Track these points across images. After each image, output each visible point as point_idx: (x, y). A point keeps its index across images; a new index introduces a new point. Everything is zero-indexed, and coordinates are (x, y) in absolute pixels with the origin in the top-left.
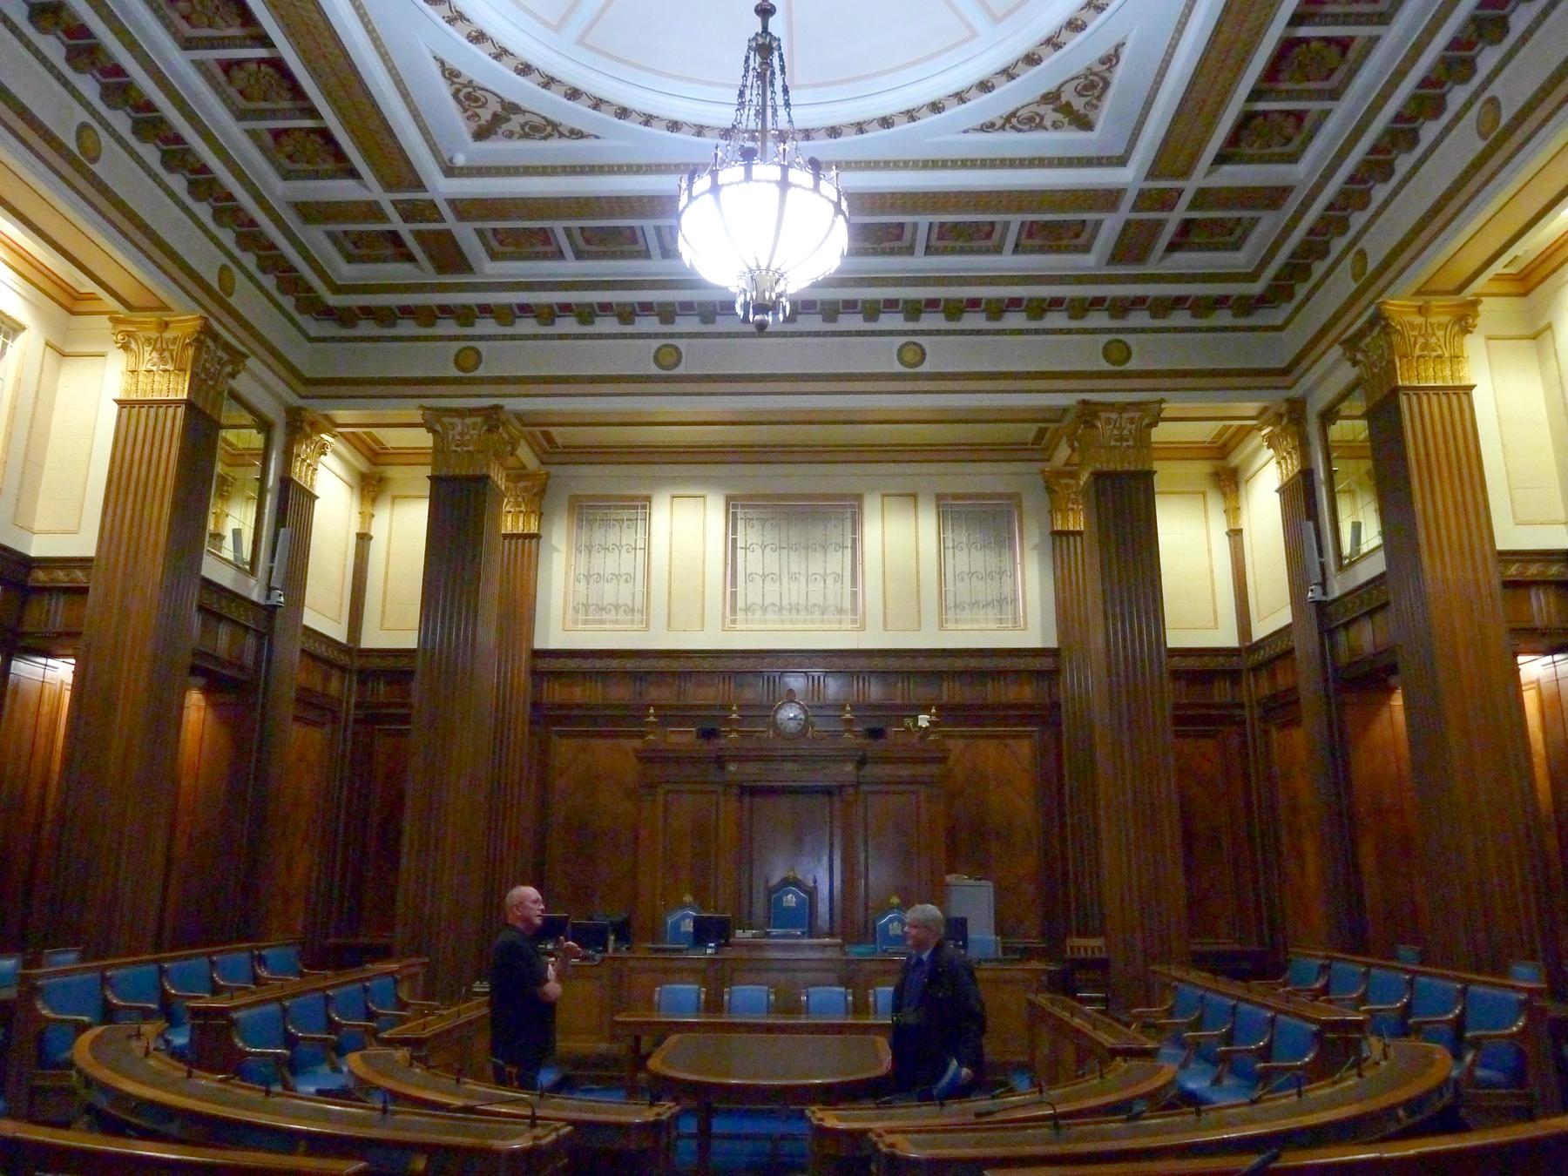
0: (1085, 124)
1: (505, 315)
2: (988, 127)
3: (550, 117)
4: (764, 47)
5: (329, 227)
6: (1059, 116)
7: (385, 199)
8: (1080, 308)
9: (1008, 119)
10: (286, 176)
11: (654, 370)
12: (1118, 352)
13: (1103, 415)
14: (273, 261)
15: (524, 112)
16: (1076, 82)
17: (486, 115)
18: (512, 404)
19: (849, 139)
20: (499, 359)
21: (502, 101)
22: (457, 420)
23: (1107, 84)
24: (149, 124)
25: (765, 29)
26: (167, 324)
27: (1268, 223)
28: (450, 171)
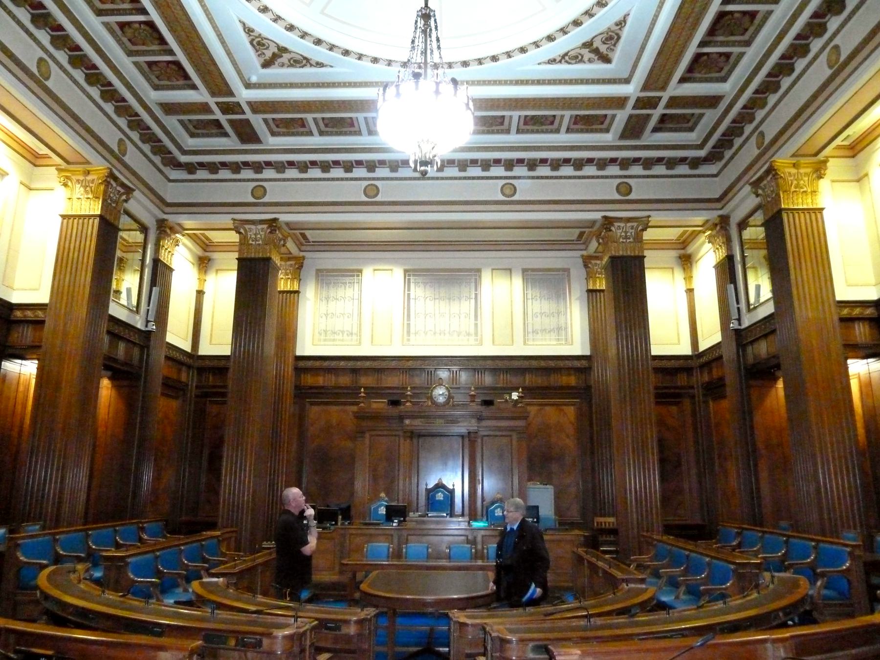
0: (606, 60)
1: (280, 167)
2: (552, 61)
3: (305, 55)
6: (592, 56)
7: (212, 101)
8: (602, 164)
9: (563, 57)
12: (625, 189)
13: (616, 224)
14: (148, 137)
15: (290, 52)
17: (268, 54)
20: (275, 192)
22: (253, 227)
23: (619, 38)
24: (79, 60)
28: (248, 86)
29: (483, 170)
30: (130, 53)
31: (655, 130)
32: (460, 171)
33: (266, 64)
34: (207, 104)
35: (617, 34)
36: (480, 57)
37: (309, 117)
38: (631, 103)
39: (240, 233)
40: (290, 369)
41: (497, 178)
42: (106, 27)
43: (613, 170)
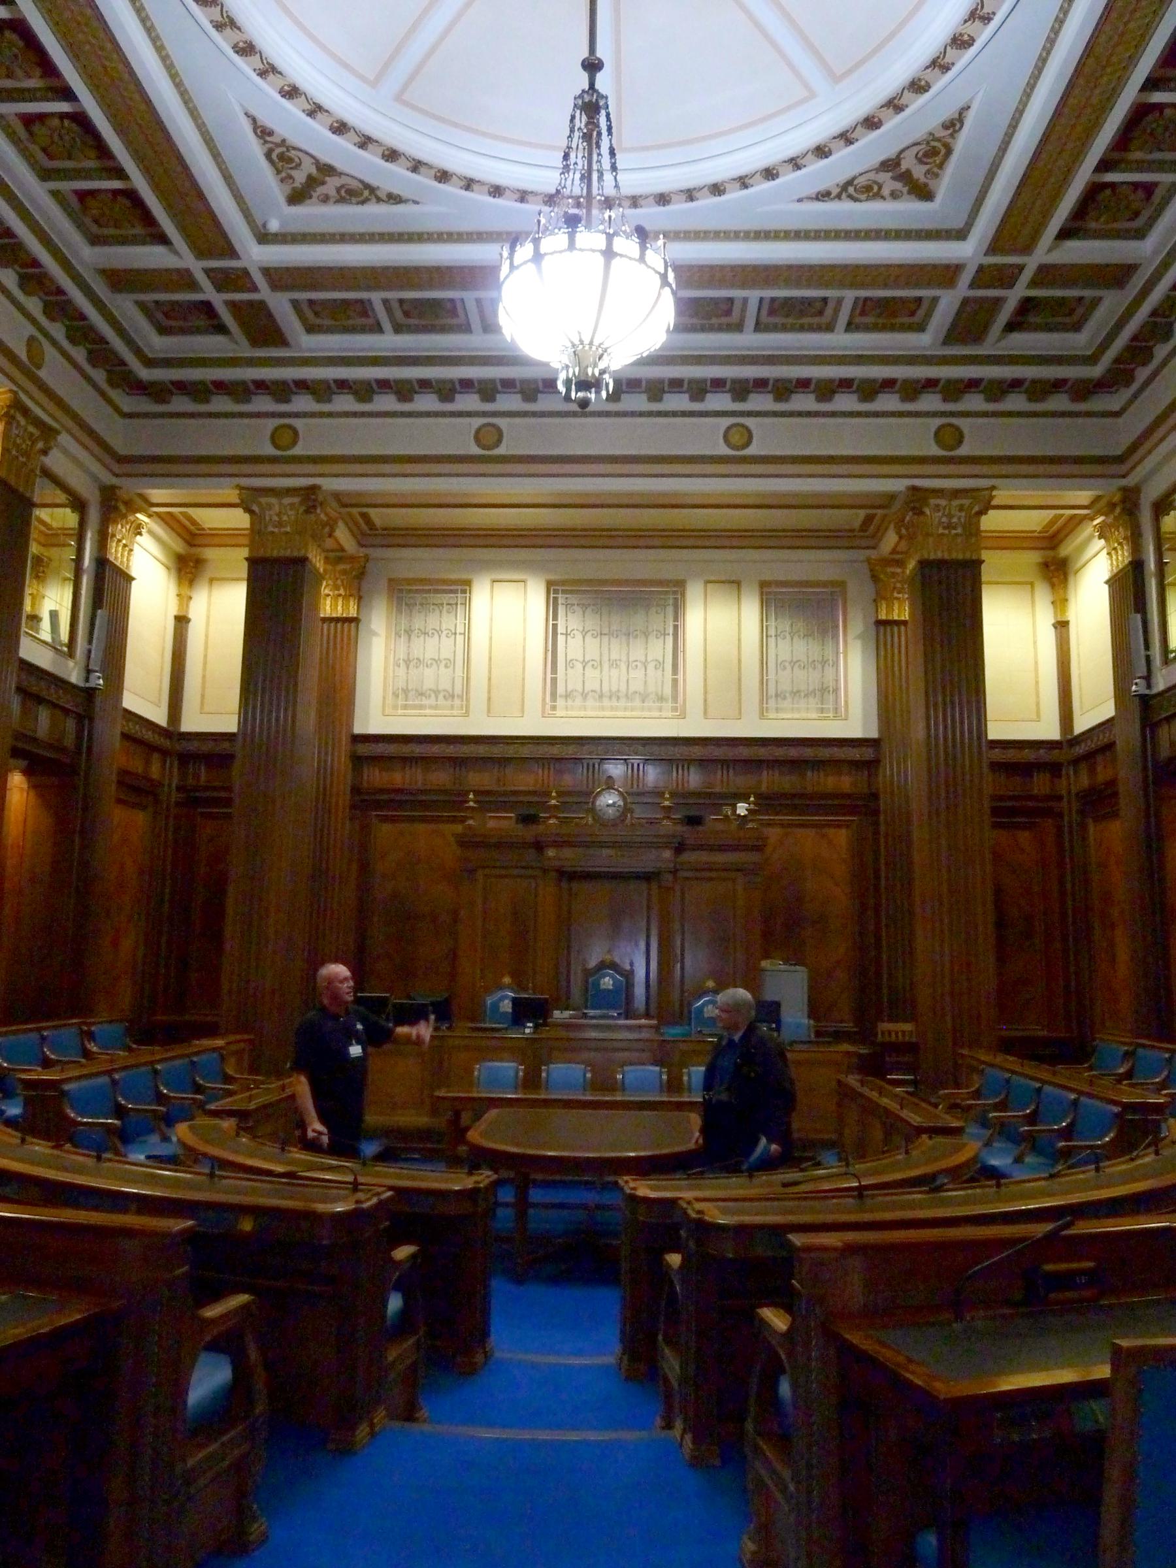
0: (924, 193)
1: (321, 391)
6: (898, 185)
7: (196, 267)
8: (913, 390)
12: (950, 436)
14: (81, 331)
15: (341, 174)
17: (300, 177)
18: (330, 484)
19: (679, 207)
22: (273, 500)
27: (1111, 302)
28: (264, 237)
30: (45, 175)
31: (1012, 327)
33: (297, 197)
34: (187, 271)
38: (966, 278)
43: (719, 401)
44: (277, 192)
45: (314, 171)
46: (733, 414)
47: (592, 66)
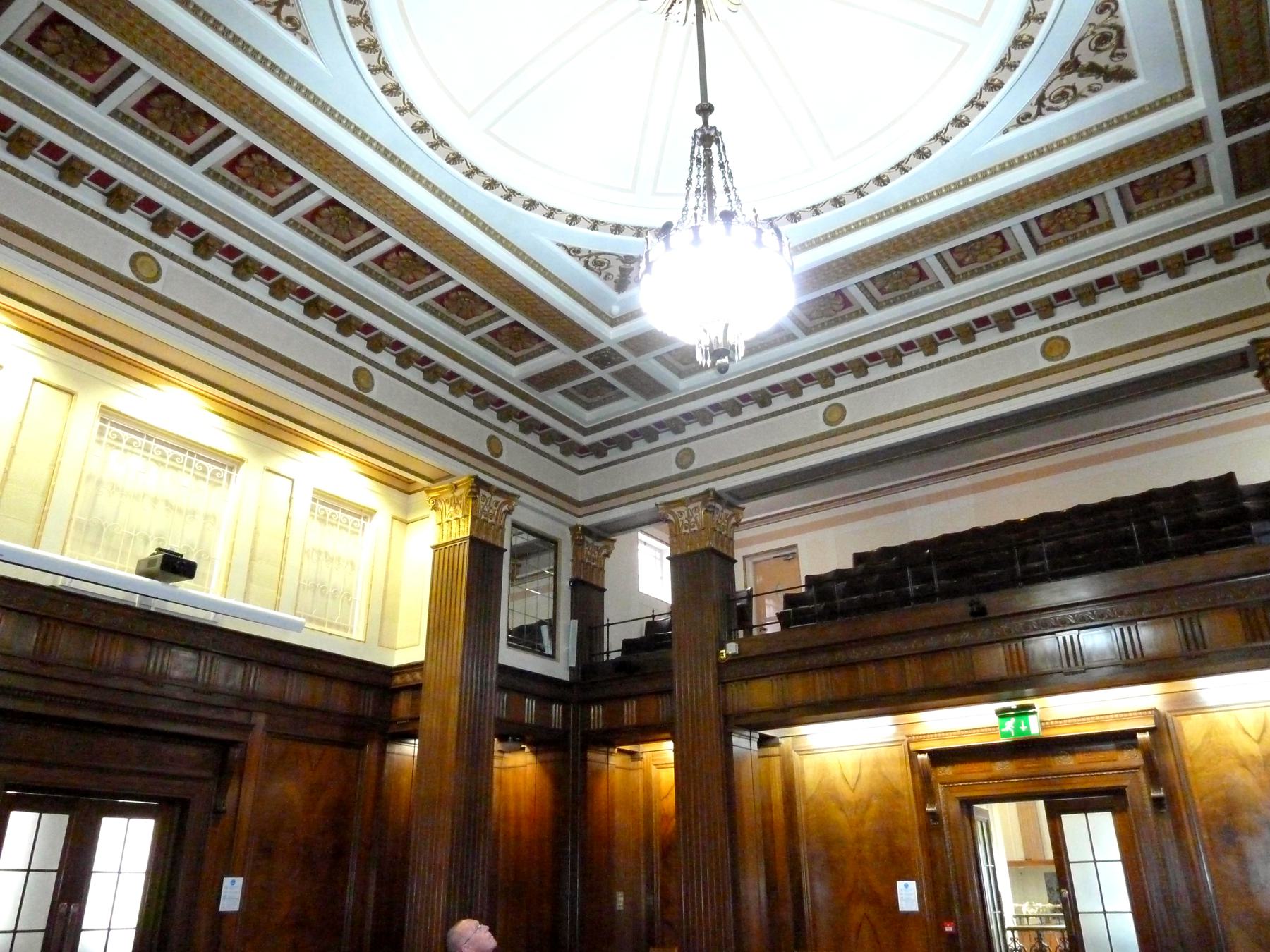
0: (1125, 75)
1: (703, 417)
2: (1023, 119)
4: (707, 138)
5: (563, 387)
6: (1091, 80)
7: (579, 357)
9: (1040, 101)
10: (515, 362)
11: (825, 428)
12: (1054, 348)
14: (529, 425)
16: (1086, 42)
17: (616, 273)
18: (720, 486)
19: (898, 181)
20: (705, 454)
21: (619, 257)
22: (683, 509)
23: (1121, 32)
24: (406, 358)
25: (706, 123)
26: (456, 486)
28: (613, 322)
29: (1003, 330)
32: (927, 354)
35: (1113, 27)
36: (858, 184)
37: (927, 255)
38: (1216, 126)
39: (668, 521)
40: (1148, 803)
41: (1030, 335)
42: (427, 310)
44: (608, 289)
45: (622, 264)
46: (1046, 330)
47: (705, 110)
